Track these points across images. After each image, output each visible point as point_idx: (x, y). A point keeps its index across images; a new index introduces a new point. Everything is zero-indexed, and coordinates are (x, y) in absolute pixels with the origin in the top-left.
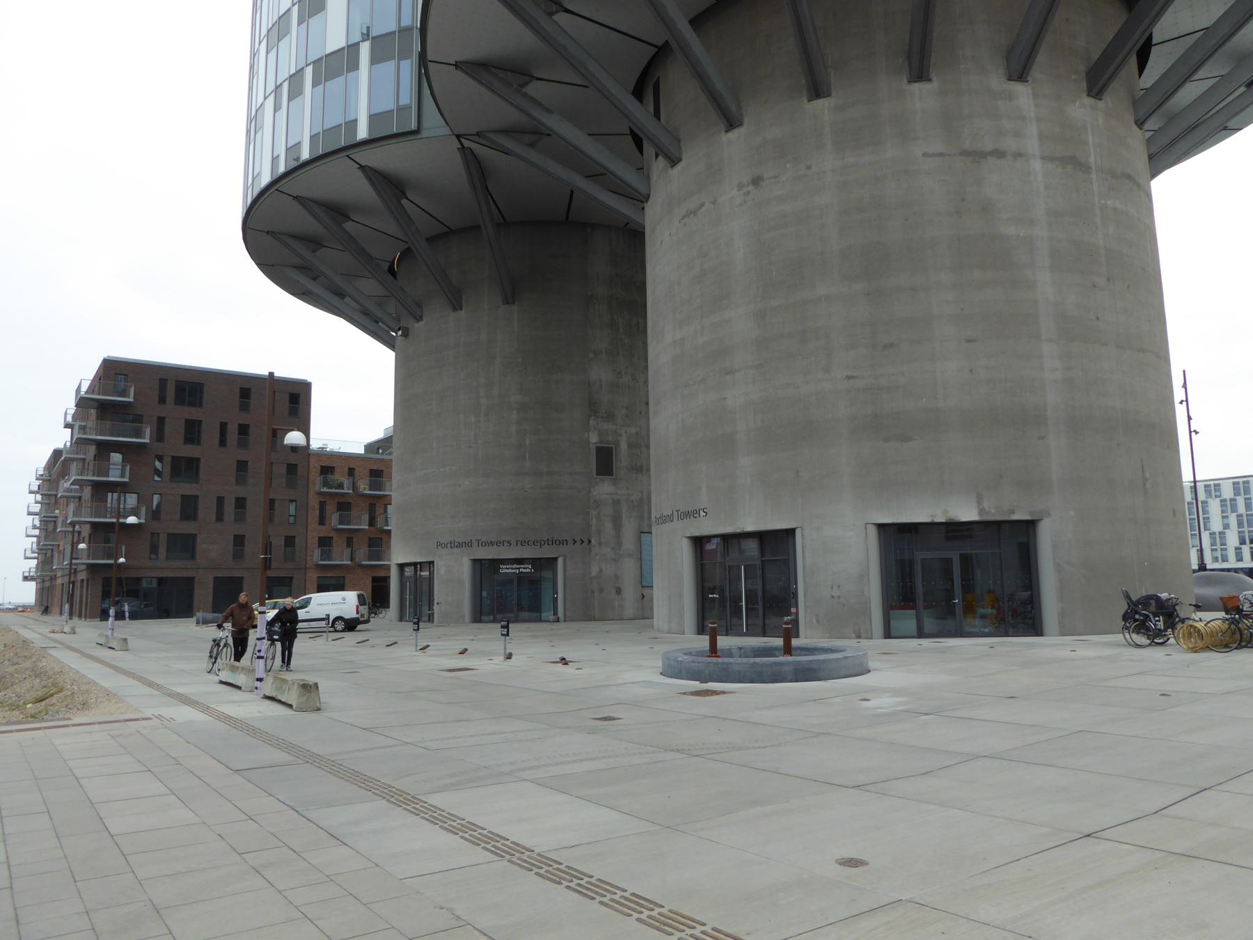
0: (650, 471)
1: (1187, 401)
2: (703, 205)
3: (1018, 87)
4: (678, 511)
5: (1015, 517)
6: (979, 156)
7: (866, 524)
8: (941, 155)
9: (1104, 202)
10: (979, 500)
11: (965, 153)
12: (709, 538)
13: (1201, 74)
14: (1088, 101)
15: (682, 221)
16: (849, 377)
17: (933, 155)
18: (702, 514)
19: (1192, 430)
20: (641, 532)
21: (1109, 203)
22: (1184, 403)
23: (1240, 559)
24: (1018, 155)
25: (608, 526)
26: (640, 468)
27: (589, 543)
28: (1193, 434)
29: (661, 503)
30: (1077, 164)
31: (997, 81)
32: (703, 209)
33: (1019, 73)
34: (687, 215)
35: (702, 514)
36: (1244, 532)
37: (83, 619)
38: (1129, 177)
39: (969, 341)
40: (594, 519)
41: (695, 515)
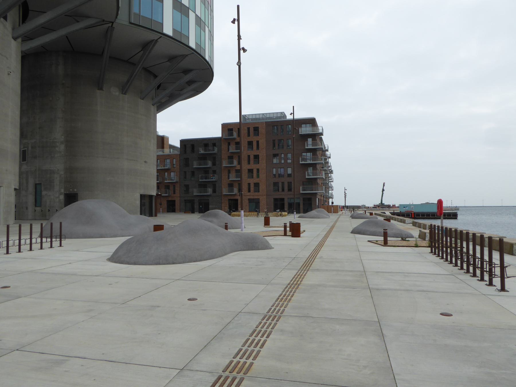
1: (293, 114)
7: (288, 198)
19: (241, 47)
22: (292, 114)
28: (242, 51)
37: (485, 236)
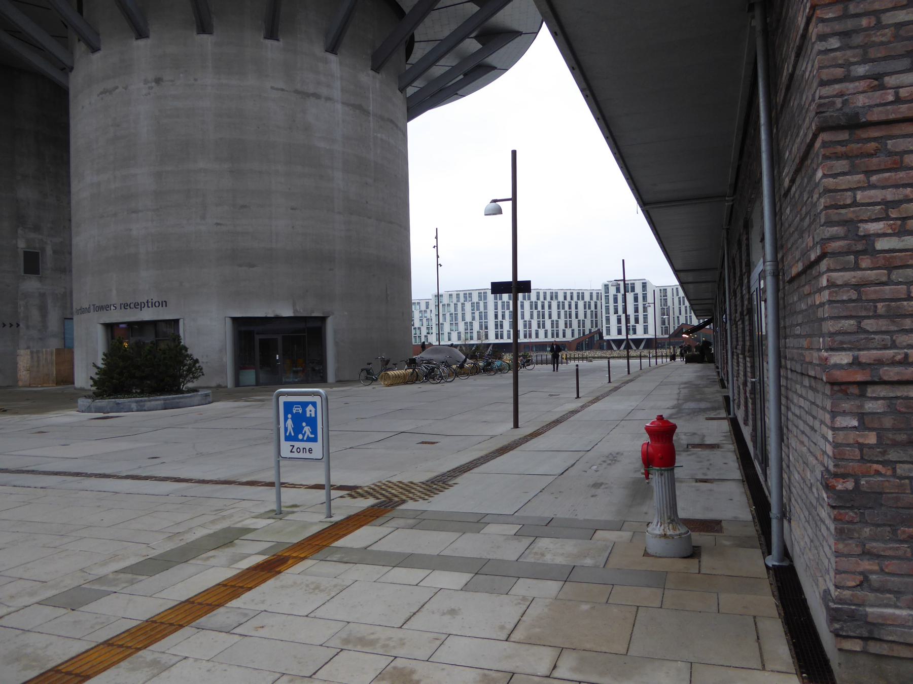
0: (72, 272)
1: (437, 247)
2: (117, 88)
3: (331, 57)
4: (94, 305)
5: (314, 315)
6: (305, 95)
8: (282, 90)
9: (376, 134)
10: (294, 305)
11: (297, 92)
12: (118, 324)
13: (442, 62)
14: (371, 73)
15: (101, 96)
16: (217, 224)
17: (277, 89)
18: (112, 308)
20: (65, 318)
21: (379, 135)
22: (436, 247)
23: (537, 336)
24: (328, 99)
25: (35, 314)
26: (64, 269)
27: (17, 327)
28: (439, 266)
29: (81, 298)
30: (361, 109)
31: (318, 50)
32: (117, 91)
33: (333, 49)
34: (105, 92)
35: (112, 308)
36: (482, 322)
38: (392, 121)
39: (292, 209)
40: (22, 308)
41: (107, 309)
